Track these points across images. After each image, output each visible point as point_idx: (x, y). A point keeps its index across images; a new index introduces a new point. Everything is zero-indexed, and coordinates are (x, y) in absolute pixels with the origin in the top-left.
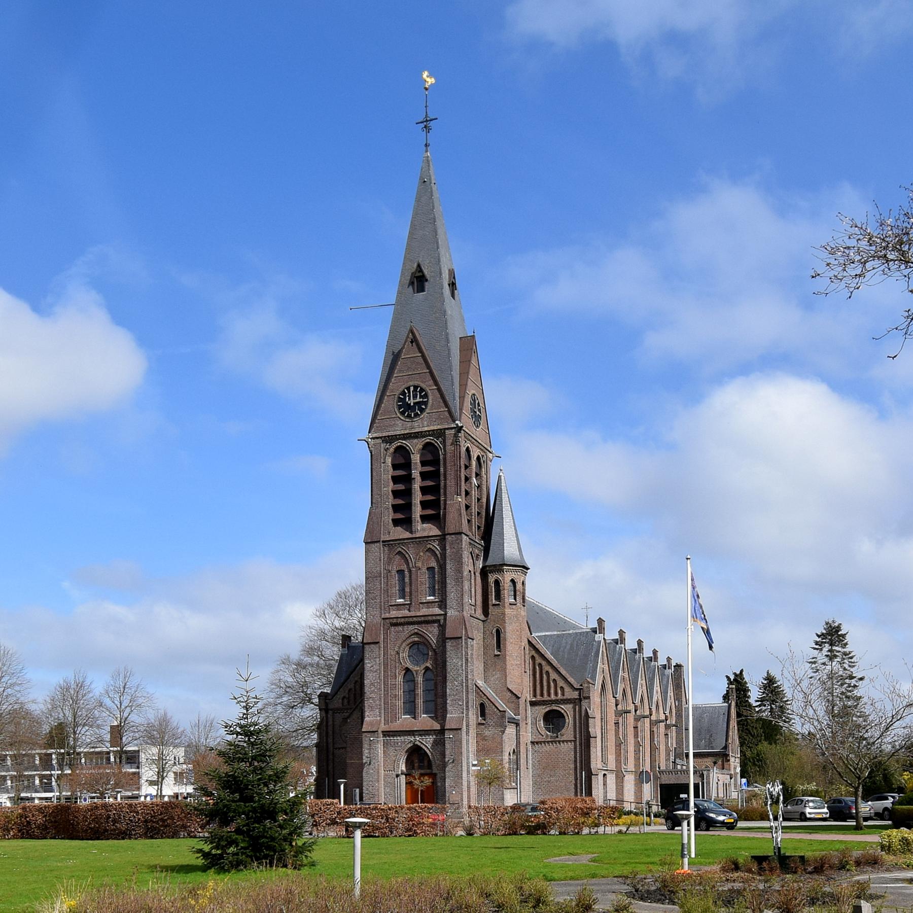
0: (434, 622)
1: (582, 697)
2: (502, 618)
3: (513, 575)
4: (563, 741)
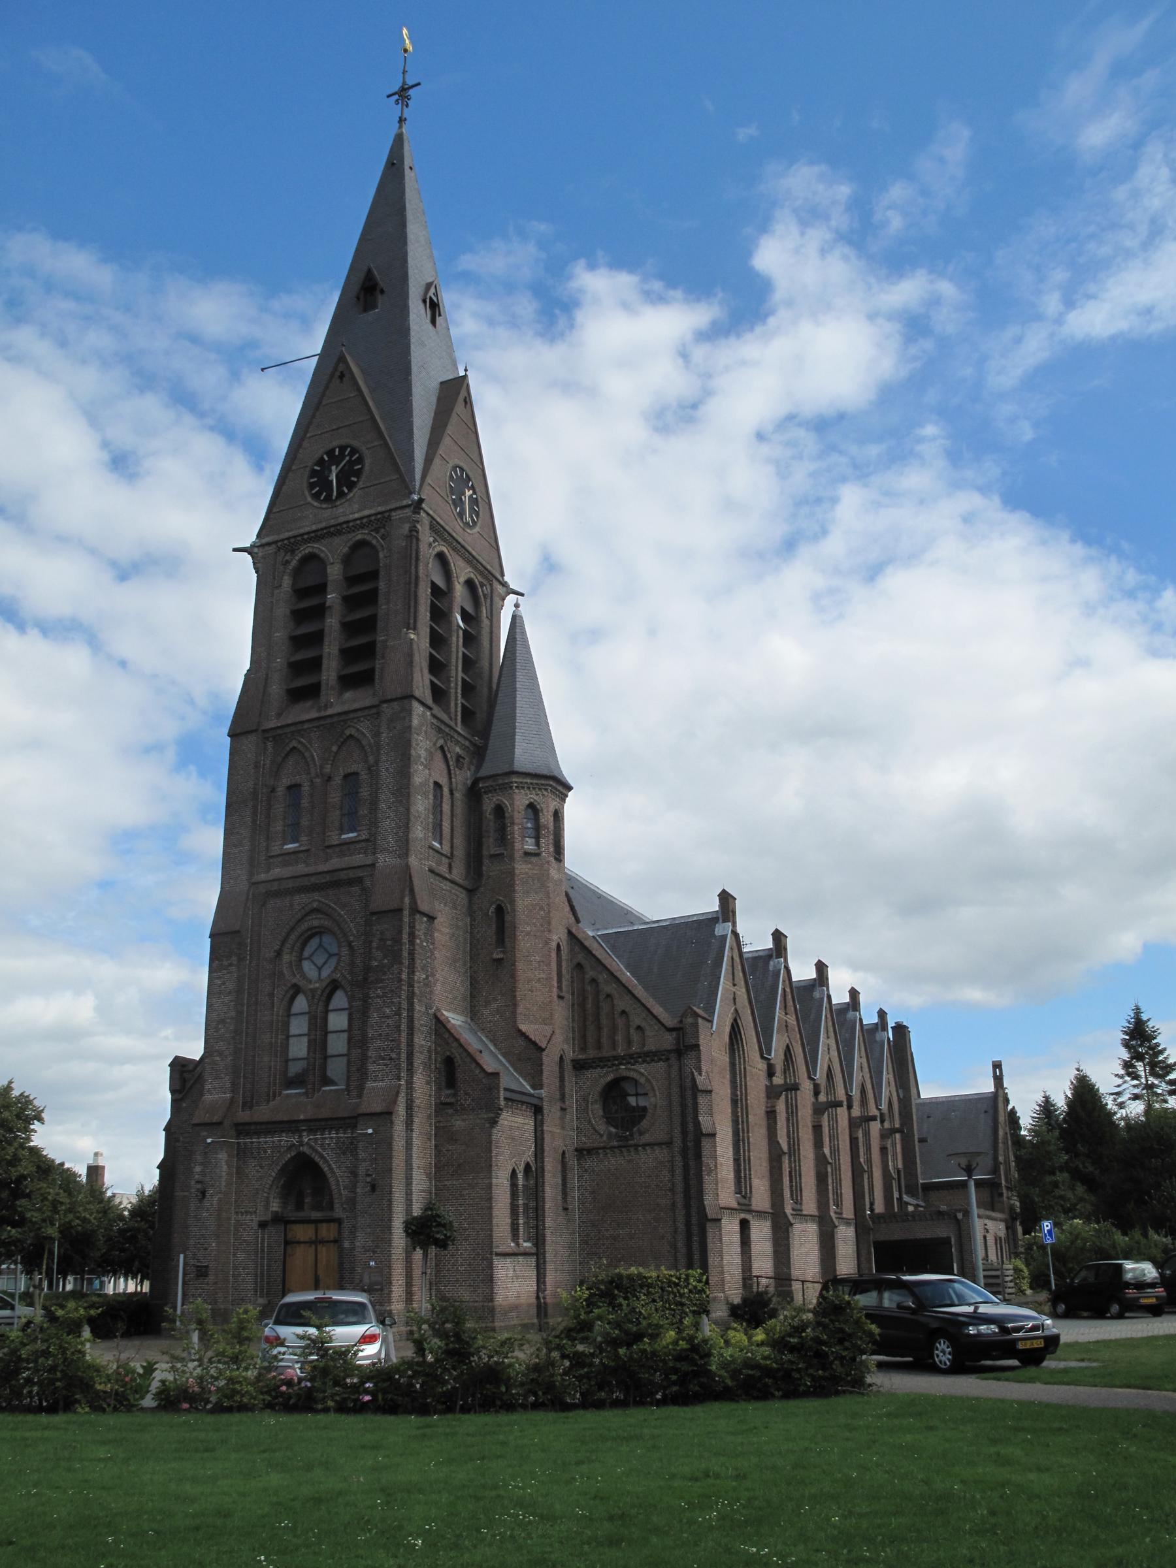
0: (351, 882)
1: (684, 1046)
2: (508, 884)
3: (533, 797)
4: (644, 1146)
